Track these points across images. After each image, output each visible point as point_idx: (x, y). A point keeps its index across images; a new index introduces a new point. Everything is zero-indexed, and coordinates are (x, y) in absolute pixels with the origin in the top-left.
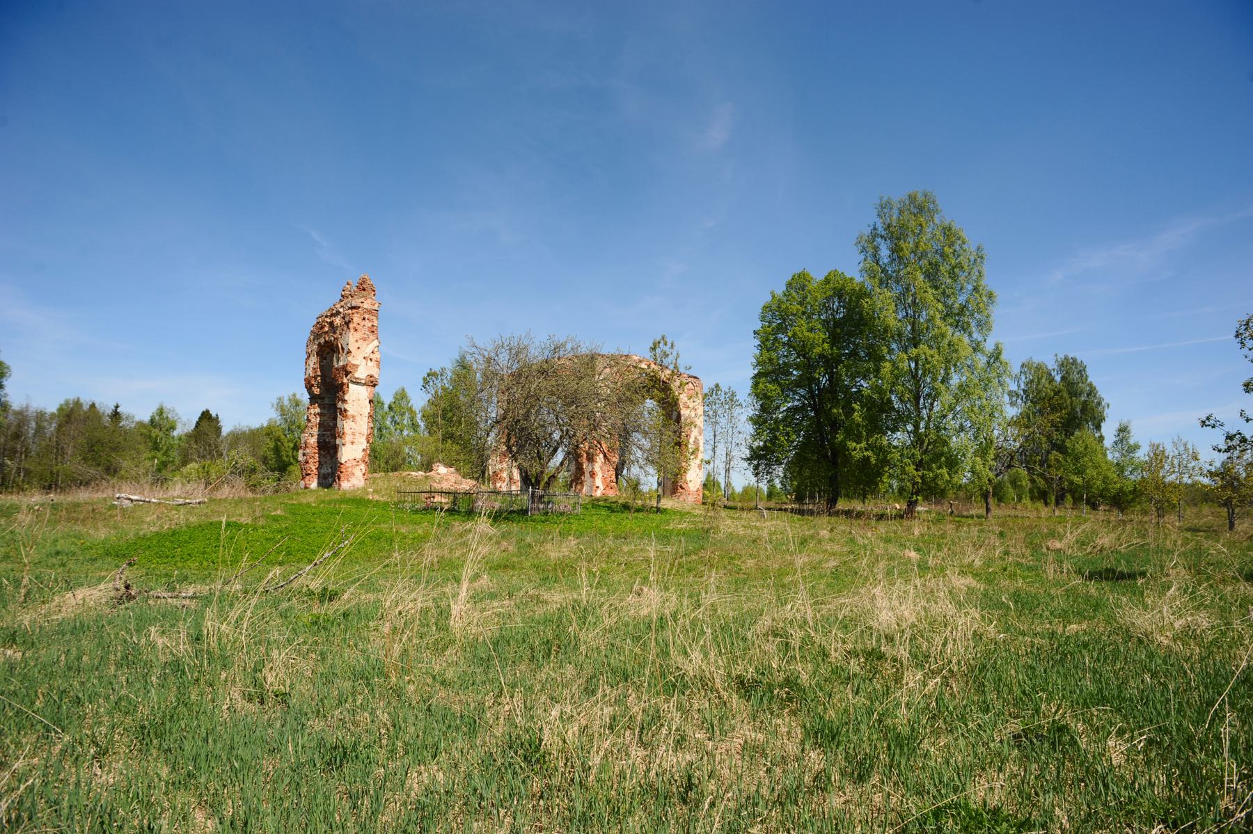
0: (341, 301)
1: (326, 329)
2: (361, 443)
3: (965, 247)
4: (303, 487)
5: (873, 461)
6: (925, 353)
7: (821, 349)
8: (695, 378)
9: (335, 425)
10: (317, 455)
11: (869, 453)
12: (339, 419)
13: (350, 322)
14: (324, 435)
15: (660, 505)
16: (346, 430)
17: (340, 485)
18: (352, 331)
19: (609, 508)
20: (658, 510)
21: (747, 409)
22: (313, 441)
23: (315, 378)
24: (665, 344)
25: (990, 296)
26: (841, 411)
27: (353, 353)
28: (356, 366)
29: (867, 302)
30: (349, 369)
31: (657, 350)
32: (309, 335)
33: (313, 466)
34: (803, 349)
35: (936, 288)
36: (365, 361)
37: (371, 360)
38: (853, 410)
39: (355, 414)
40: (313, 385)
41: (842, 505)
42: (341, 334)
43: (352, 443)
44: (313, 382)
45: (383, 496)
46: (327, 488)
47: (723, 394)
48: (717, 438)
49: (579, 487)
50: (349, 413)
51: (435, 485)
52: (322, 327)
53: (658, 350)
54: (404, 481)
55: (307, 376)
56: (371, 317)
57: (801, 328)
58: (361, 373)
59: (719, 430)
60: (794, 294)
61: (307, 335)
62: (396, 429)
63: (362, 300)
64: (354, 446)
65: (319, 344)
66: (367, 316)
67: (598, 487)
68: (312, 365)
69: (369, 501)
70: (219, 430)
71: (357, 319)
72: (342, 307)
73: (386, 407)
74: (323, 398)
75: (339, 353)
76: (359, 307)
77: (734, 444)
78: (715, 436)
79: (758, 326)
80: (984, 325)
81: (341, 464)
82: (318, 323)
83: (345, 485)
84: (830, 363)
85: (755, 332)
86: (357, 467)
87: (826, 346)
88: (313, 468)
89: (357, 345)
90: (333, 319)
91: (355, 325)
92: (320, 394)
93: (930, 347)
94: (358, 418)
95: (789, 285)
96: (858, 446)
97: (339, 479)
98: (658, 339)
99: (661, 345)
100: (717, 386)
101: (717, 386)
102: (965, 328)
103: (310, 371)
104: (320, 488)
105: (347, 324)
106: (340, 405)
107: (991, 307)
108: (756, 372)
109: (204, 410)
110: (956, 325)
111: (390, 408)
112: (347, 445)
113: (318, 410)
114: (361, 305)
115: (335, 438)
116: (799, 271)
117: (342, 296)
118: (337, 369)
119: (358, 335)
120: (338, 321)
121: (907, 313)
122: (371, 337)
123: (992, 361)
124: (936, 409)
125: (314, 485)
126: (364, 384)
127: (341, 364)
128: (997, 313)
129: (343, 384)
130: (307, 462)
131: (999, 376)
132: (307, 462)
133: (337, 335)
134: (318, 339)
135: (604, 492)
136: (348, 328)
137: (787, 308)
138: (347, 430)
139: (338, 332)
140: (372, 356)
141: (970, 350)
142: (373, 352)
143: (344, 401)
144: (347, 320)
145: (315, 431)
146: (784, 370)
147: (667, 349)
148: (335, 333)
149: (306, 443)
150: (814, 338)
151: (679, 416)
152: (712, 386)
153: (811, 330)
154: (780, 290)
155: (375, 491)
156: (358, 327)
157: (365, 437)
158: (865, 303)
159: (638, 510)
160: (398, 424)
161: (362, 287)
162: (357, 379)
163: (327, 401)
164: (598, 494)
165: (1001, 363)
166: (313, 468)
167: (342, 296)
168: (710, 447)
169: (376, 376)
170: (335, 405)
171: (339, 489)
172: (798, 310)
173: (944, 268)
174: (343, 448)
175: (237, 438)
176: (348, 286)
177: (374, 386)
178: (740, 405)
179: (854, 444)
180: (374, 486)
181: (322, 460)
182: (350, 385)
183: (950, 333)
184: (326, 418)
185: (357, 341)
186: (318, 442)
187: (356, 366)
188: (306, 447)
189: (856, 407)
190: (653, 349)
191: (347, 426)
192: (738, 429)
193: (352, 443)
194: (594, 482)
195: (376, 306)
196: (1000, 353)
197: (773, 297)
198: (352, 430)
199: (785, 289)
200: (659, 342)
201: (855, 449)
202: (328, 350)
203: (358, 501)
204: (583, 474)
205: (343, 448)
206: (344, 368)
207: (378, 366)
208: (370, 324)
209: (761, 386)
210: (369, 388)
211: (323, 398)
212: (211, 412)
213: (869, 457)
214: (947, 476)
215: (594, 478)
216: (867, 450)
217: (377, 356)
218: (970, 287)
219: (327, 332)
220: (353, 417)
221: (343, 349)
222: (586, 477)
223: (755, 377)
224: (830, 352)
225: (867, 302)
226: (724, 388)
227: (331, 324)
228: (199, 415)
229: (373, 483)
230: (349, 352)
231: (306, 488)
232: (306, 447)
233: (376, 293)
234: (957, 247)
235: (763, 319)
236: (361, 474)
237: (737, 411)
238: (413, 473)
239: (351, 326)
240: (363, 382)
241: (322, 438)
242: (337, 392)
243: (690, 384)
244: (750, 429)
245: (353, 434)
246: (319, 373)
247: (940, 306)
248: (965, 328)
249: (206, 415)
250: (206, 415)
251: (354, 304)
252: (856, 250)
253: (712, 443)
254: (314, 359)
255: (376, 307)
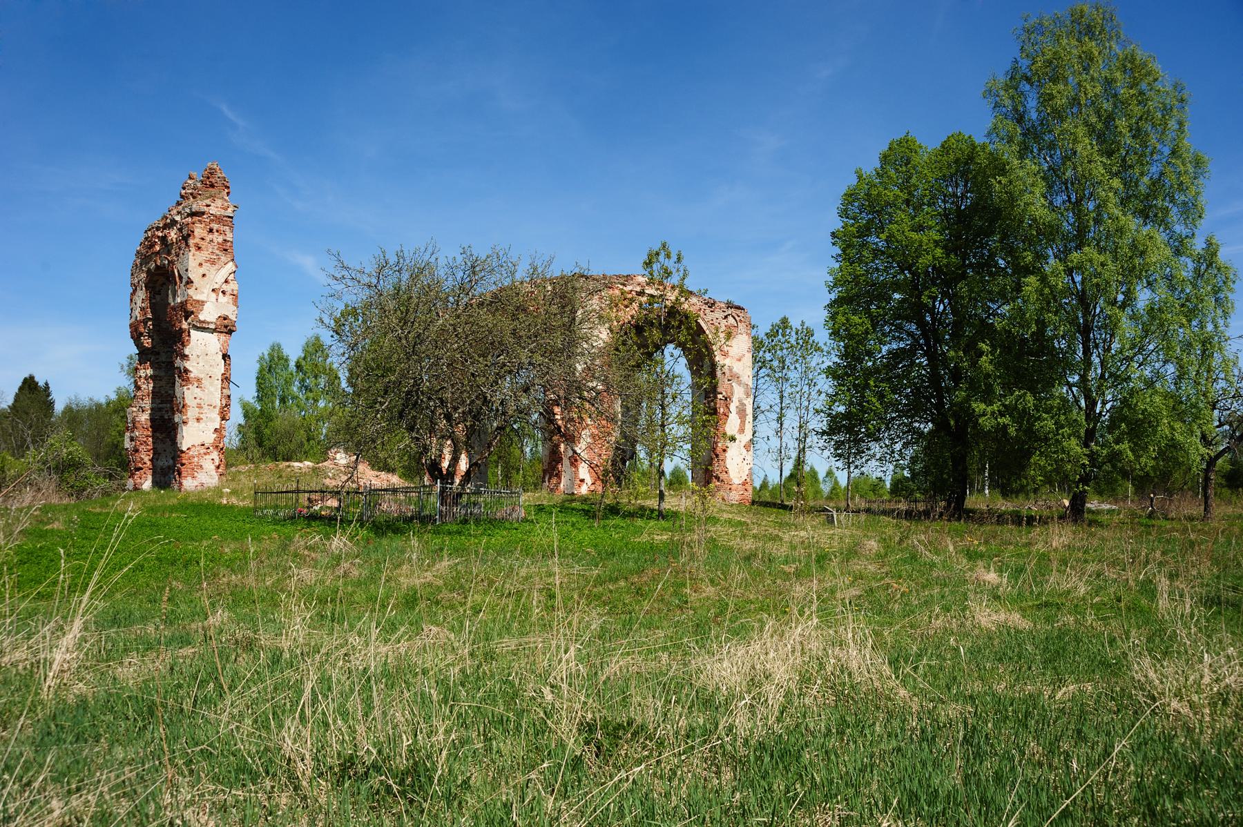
0: (179, 204)
1: (157, 248)
2: (212, 420)
3: (1158, 86)
4: (131, 488)
5: (1012, 431)
6: (1091, 261)
7: (930, 257)
8: (738, 308)
9: (174, 396)
10: (150, 439)
11: (1005, 420)
12: (177, 384)
13: (189, 235)
14: (160, 409)
15: (662, 508)
16: (187, 401)
17: (181, 484)
18: (193, 249)
19: (586, 513)
20: (662, 515)
21: (828, 355)
22: (144, 418)
23: (145, 322)
24: (668, 256)
25: (1198, 163)
26: (961, 354)
27: (196, 284)
28: (202, 303)
29: (1000, 182)
30: (190, 307)
31: (655, 266)
32: (134, 258)
33: (146, 457)
34: (903, 257)
35: (1110, 154)
36: (213, 295)
37: (224, 292)
38: (981, 354)
39: (201, 376)
40: (141, 334)
41: (973, 501)
42: (178, 256)
43: (198, 420)
44: (142, 330)
45: (243, 500)
46: (164, 488)
47: (793, 333)
48: (786, 401)
49: (554, 480)
50: (192, 375)
51: (327, 481)
52: (152, 245)
53: (656, 267)
54: (281, 477)
55: (133, 320)
56: (222, 228)
57: (901, 224)
58: (209, 314)
59: (788, 390)
60: (892, 173)
61: (131, 259)
62: (307, 399)
63: (208, 202)
64: (202, 425)
65: (149, 271)
66: (215, 226)
67: (582, 481)
68: (139, 303)
69: (220, 506)
70: (50, 405)
71: (199, 230)
72: (179, 213)
73: (292, 364)
74: (158, 353)
75: (176, 284)
76: (203, 213)
77: (811, 412)
78: (782, 397)
79: (837, 224)
80: (1191, 211)
81: (183, 452)
82: (146, 239)
83: (189, 484)
84: (946, 279)
85: (833, 235)
86: (207, 457)
87: (939, 252)
88: (146, 459)
89: (202, 271)
90: (166, 231)
91: (197, 240)
92: (153, 347)
93: (1101, 250)
94: (205, 382)
95: (885, 159)
96: (989, 409)
97: (180, 474)
98: (656, 248)
99: (661, 258)
100: (785, 321)
101: (785, 321)
102: (1162, 221)
103: (137, 312)
104: (156, 489)
105: (186, 238)
106: (178, 363)
107: (1201, 181)
108: (833, 296)
109: (27, 375)
110: (1145, 214)
111: (298, 366)
112: (190, 423)
113: (150, 372)
114: (206, 209)
115: (174, 414)
116: (900, 135)
117: (182, 197)
118: (174, 308)
119: (203, 256)
120: (173, 235)
121: (1069, 197)
122: (223, 258)
123: (1203, 267)
124: (1115, 346)
125: (147, 485)
126: (214, 331)
127: (179, 300)
128: (1208, 191)
129: (181, 331)
130: (137, 451)
131: (1217, 291)
132: (137, 451)
133: (172, 257)
134: (147, 263)
135: (593, 488)
136: (187, 245)
137: (879, 195)
138: (189, 400)
139: (173, 252)
140: (225, 287)
141: (1168, 252)
142: (226, 281)
143: (185, 357)
144: (185, 232)
145: (147, 403)
146: (879, 293)
147: (670, 264)
148: (169, 253)
149: (134, 422)
150: (921, 242)
151: (713, 365)
152: (777, 321)
153: (919, 228)
154: (871, 165)
155: (234, 492)
156: (201, 243)
157: (217, 410)
158: (997, 184)
159: (631, 515)
160: (311, 391)
161: (210, 183)
162: (204, 322)
163: (163, 358)
164: (584, 490)
165: (1219, 269)
166: (146, 459)
167: (182, 197)
168: (775, 416)
169: (233, 318)
170: (172, 363)
171: (180, 490)
172: (896, 197)
173: (1122, 124)
174: (184, 428)
175: (73, 416)
176: (190, 182)
177: (230, 332)
178: (818, 349)
179: (983, 406)
180: (233, 485)
181: (160, 447)
182: (192, 331)
183: (1133, 227)
184: (163, 383)
185: (201, 265)
186: (152, 420)
187: (202, 303)
188: (135, 427)
189: (984, 347)
190: (648, 264)
191: (190, 395)
192: (817, 388)
193: (198, 420)
194: (576, 473)
195: (230, 210)
196: (1214, 254)
197: (860, 177)
198: (198, 401)
199: (879, 166)
200: (657, 254)
201: (984, 414)
202: (162, 280)
203: (203, 507)
204: (560, 460)
205: (184, 428)
206: (183, 305)
207: (235, 303)
208: (220, 239)
209: (841, 318)
210: (223, 337)
211: (158, 353)
212: (36, 379)
213: (1005, 426)
214: (1130, 453)
215: (576, 467)
216: (1002, 415)
217: (233, 286)
218: (1167, 151)
219: (158, 253)
220: (199, 380)
221: (181, 277)
222: (565, 466)
223: (831, 305)
224: (945, 261)
225: (1000, 182)
226: (795, 323)
227: (164, 239)
228: (20, 384)
229: (233, 480)
230: (190, 282)
231: (136, 489)
232: (135, 427)
233: (231, 190)
234: (1144, 86)
235: (844, 213)
236: (213, 467)
237: (813, 359)
238: (296, 464)
239: (191, 242)
240: (212, 326)
241: (159, 414)
242: (175, 343)
243: (730, 318)
244: (826, 385)
245: (199, 406)
246: (150, 316)
247: (1116, 183)
248: (1162, 221)
249: (29, 384)
250: (29, 384)
251: (195, 208)
252: (987, 105)
253: (779, 410)
254: (141, 294)
255: (229, 212)
